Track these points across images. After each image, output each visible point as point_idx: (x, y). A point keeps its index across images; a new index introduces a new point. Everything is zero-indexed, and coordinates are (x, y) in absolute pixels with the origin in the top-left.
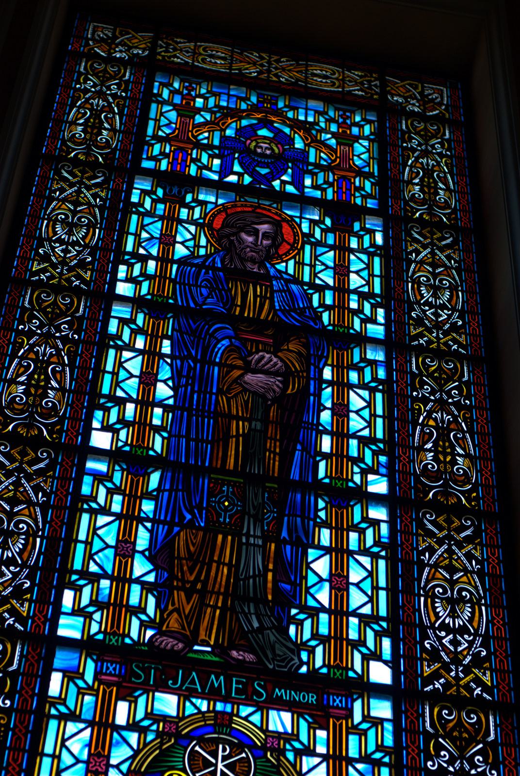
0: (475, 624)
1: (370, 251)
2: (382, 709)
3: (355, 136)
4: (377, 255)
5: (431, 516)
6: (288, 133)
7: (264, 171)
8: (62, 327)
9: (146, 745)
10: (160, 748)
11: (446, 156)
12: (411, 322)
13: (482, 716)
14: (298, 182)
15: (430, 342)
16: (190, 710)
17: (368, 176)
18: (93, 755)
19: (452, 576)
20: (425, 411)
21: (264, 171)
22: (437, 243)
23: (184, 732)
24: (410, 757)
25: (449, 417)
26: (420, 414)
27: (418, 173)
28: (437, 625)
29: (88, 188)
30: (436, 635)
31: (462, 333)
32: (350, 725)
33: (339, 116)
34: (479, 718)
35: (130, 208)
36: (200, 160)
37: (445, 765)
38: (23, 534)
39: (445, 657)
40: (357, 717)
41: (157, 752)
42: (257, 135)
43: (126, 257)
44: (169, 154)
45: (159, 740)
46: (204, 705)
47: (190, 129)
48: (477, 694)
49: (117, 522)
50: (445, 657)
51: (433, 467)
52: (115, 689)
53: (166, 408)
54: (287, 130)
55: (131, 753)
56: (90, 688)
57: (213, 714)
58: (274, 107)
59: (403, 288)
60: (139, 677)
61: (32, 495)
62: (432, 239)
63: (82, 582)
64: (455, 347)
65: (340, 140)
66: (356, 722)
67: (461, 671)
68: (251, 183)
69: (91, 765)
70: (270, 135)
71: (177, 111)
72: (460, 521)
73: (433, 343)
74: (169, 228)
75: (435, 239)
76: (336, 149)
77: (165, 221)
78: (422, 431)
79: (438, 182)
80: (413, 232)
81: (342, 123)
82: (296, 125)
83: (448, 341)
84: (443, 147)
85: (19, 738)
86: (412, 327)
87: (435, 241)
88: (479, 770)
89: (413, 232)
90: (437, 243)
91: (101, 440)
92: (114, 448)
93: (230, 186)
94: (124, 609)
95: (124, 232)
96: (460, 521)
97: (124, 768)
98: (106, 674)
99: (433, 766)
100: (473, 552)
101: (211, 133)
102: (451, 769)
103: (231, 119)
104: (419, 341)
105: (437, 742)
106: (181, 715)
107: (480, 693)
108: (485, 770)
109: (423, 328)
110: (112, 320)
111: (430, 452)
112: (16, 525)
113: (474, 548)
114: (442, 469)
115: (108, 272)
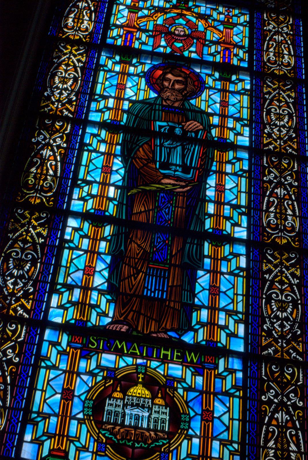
0: (294, 316)
1: (239, 174)
2: (236, 364)
3: (234, 24)
4: (246, 95)
5: (271, 251)
6: (195, 22)
7: (179, 45)
8: (7, 352)
9: (96, 383)
10: (104, 385)
11: (290, 34)
12: (263, 333)
13: (296, 369)
14: (200, 52)
15: (275, 148)
16: (122, 364)
17: (242, 47)
18: (87, 266)
19: (279, 104)
20: (270, 412)
21: (179, 45)
22: (282, 87)
23: (118, 377)
24: (253, 290)
25: (287, 416)
26: (267, 190)
27: (273, 45)
28: (272, 316)
29: (75, 56)
30: (271, 128)
31: (300, 341)
32: (216, 373)
33: (225, 11)
34: (294, 371)
35: (99, 67)
36: (140, 39)
37: (272, 398)
38: (72, 78)
39: (275, 335)
40: (221, 368)
41: (103, 387)
42: (175, 23)
43: (96, 97)
44: (122, 35)
45: (104, 381)
46: (129, 360)
47: (136, 20)
48: (294, 356)
49: (85, 255)
50: (275, 335)
51: (273, 59)
52: (79, 351)
53: (117, 187)
54: (194, 20)
55: (88, 388)
56: (65, 351)
57: (135, 367)
58: (186, 6)
59: (259, 304)
60: (93, 345)
61: (36, 238)
62: (281, 260)
63: (63, 290)
64: (290, 150)
65: (225, 26)
66: (220, 372)
67: (285, 343)
68: (171, 52)
69: (86, 271)
70: (184, 23)
71: (128, 9)
72: (289, 255)
73: (277, 148)
74: (91, 260)
75: (284, 259)
76: (223, 31)
77: (67, 374)
78: (267, 429)
79: (290, 442)
80: (267, 81)
81: (227, 15)
82: (200, 16)
83: (289, 350)
84: (288, 28)
85: (38, 307)
86: (265, 138)
87: (284, 261)
88: (292, 401)
89: (267, 81)
90: (282, 87)
91: (76, 205)
92: (101, 121)
93: (159, 54)
94: (65, 438)
95: (95, 82)
96: (289, 255)
97: (83, 397)
98: (74, 343)
99: (265, 398)
100: (296, 272)
101: (148, 22)
102: (276, 401)
103: (160, 14)
104: (268, 350)
105: (268, 384)
106: (117, 367)
107: (295, 356)
108: (296, 401)
109: (272, 339)
110: (44, 343)
111: (272, 450)
112: (26, 256)
113: (295, 270)
114: (279, 223)
115: (35, 344)
